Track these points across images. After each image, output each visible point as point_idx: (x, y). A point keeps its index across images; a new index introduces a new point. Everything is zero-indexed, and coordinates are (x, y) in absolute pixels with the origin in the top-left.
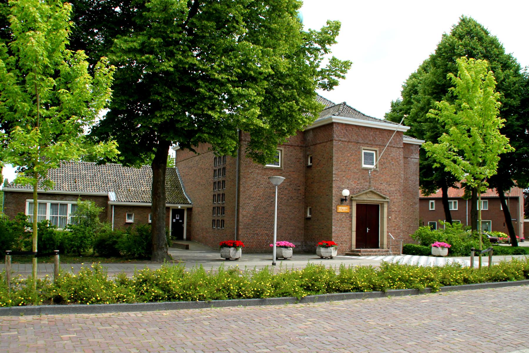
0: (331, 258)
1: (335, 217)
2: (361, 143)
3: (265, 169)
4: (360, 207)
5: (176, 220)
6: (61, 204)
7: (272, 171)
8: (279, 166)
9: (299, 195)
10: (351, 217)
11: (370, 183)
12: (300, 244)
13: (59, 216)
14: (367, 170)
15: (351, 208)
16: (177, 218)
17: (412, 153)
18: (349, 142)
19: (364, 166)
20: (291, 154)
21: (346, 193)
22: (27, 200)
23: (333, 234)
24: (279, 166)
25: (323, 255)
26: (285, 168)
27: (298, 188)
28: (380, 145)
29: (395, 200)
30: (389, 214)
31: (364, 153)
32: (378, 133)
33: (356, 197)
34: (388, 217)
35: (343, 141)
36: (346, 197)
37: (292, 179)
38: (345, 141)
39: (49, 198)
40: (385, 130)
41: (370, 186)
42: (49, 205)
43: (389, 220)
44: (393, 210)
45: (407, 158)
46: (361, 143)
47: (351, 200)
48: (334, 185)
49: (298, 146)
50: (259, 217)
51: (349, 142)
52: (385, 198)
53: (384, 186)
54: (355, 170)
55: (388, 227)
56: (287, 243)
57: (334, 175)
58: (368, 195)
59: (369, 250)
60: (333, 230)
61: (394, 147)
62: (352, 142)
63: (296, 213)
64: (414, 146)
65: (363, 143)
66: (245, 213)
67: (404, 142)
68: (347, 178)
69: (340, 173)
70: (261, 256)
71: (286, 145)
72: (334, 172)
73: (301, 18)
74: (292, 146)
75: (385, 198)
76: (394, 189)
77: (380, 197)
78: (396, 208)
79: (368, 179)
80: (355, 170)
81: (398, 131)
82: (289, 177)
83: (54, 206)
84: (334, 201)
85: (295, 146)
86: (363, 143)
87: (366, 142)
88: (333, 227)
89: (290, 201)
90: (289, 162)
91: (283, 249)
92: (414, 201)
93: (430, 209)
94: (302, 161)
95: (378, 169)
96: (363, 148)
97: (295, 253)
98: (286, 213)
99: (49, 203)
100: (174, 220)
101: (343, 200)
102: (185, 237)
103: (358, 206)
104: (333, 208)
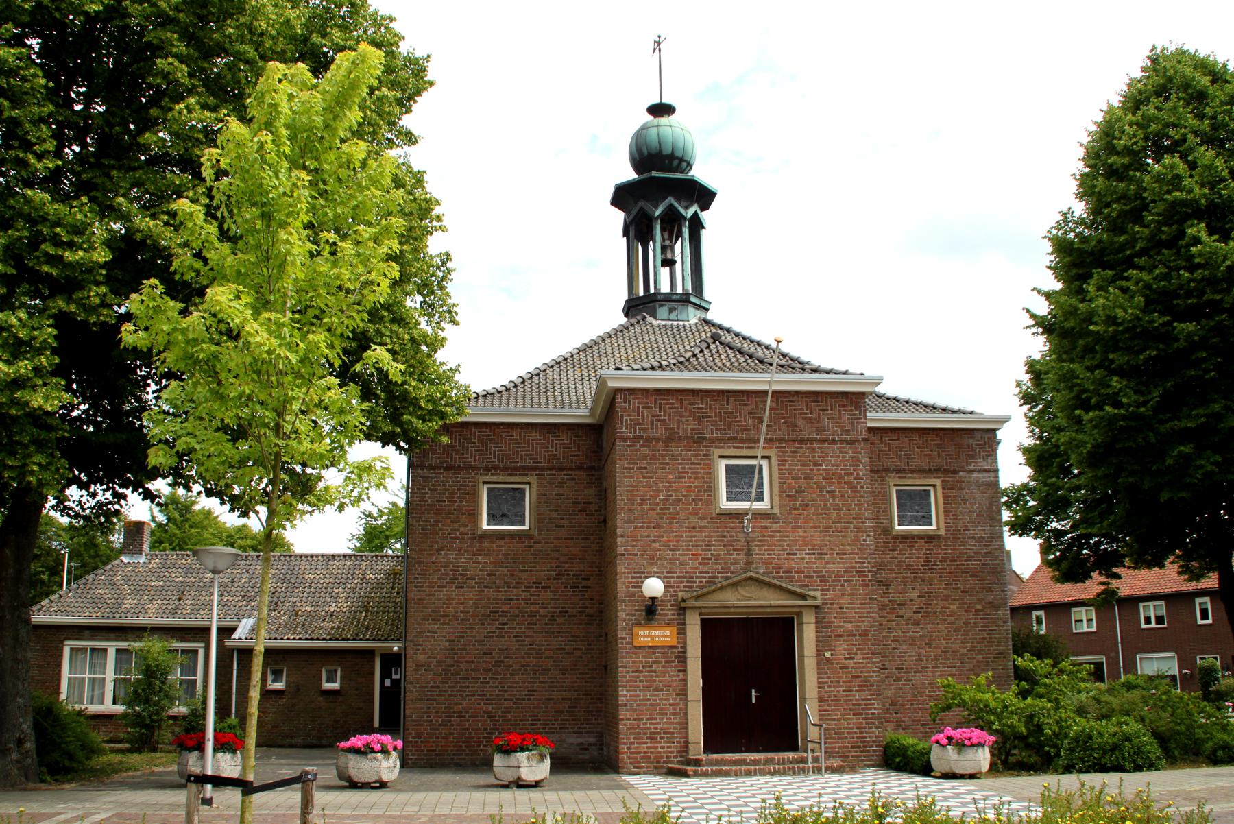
0: (382, 785)
1: (626, 663)
2: (712, 441)
3: (481, 536)
5: (393, 681)
6: (93, 650)
7: (502, 542)
8: (934, 527)
9: (587, 603)
10: (682, 657)
11: (749, 553)
12: (592, 740)
13: (87, 675)
14: (738, 515)
15: (682, 632)
16: (394, 677)
17: (973, 457)
18: (669, 439)
19: (725, 504)
20: (561, 491)
21: (654, 586)
22: (67, 643)
23: (623, 713)
24: (934, 527)
25: (356, 779)
26: (540, 530)
27: (584, 583)
28: (781, 440)
29: (846, 600)
30: (823, 643)
31: (729, 469)
33: (697, 598)
34: (819, 652)
35: (648, 440)
36: (653, 599)
37: (563, 559)
38: (657, 440)
39: (112, 636)
40: (797, 393)
41: (748, 563)
42: (111, 653)
43: (822, 662)
44: (840, 631)
45: (955, 472)
46: (712, 441)
47: (682, 610)
49: (580, 468)
50: (463, 666)
51: (669, 439)
52: (803, 597)
53: (802, 561)
54: (694, 519)
55: (820, 685)
57: (619, 540)
58: (742, 591)
59: (716, 756)
60: (622, 700)
61: (834, 442)
62: (680, 439)
63: (578, 653)
64: (978, 435)
65: (719, 440)
66: (421, 658)
67: (870, 424)
69: (643, 532)
70: (458, 778)
71: (543, 469)
73: (680, 145)
74: (561, 469)
75: (803, 597)
76: (842, 567)
78: (849, 626)
79: (741, 544)
80: (694, 519)
81: (775, 393)
82: (555, 554)
83: (124, 656)
84: (622, 615)
85: (571, 469)
86: (719, 440)
87: (732, 433)
88: (623, 692)
89: (560, 620)
90: (555, 514)
91: (351, 756)
92: (990, 599)
93: (1200, 622)
94: (593, 507)
95: (776, 511)
98: (547, 653)
99: (112, 647)
100: (388, 683)
101: (650, 610)
102: (376, 724)
103: (706, 624)
104: (621, 634)
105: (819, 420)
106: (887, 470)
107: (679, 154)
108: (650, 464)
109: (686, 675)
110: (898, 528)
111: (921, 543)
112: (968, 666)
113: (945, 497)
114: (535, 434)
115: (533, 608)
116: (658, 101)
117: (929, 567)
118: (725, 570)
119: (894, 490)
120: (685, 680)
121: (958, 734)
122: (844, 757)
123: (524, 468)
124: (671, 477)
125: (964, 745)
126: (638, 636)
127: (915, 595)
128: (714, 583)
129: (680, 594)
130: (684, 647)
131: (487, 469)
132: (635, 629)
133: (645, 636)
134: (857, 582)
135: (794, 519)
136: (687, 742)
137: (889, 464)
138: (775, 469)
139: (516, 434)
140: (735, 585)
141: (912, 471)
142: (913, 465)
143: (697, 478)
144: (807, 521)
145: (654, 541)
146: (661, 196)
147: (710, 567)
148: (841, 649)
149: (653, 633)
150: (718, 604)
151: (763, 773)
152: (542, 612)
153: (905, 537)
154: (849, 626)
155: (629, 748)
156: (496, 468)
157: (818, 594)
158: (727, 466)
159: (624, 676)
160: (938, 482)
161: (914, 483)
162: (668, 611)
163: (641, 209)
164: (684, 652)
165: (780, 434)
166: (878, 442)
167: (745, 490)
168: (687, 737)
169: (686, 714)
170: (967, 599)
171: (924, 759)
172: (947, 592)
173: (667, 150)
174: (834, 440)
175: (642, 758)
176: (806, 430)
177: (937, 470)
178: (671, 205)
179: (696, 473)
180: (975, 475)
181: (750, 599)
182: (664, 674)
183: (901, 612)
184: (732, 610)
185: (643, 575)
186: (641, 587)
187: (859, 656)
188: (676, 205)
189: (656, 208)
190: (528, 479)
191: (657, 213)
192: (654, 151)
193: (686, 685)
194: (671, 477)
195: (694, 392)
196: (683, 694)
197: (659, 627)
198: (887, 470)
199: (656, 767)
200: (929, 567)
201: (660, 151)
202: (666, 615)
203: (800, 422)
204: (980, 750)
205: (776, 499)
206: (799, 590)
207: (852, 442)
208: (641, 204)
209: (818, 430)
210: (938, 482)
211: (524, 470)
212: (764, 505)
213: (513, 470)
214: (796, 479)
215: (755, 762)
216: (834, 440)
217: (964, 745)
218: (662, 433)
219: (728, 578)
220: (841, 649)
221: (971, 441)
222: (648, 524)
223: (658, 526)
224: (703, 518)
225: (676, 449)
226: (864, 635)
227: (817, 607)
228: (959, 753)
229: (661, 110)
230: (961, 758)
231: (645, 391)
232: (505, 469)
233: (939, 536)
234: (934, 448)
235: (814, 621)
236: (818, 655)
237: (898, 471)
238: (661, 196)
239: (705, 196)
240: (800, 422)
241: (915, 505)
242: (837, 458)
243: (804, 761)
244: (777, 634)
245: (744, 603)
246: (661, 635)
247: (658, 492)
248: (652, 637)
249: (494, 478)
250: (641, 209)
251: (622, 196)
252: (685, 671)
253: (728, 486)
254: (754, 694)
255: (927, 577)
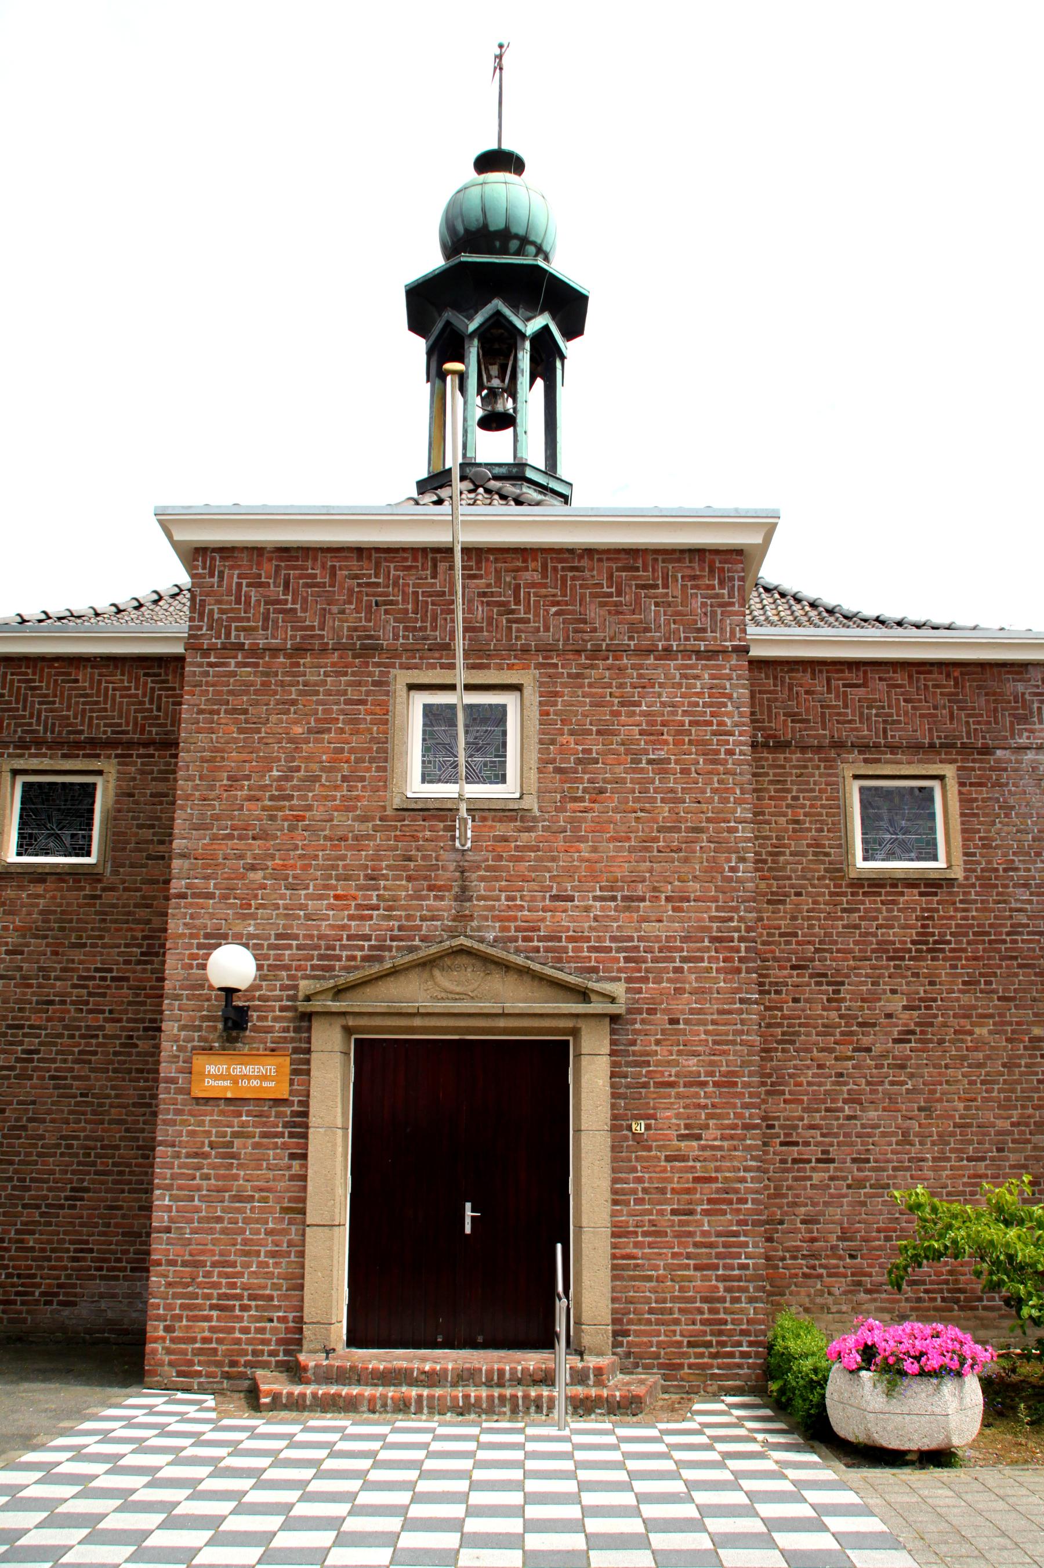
1: (176, 1132)
2: (394, 653)
4: (385, 1069)
7: (40, 889)
8: (941, 864)
10: (299, 1124)
11: (464, 895)
14: (440, 813)
15: (301, 1070)
17: (1024, 719)
18: (300, 650)
19: (415, 785)
21: (233, 965)
24: (941, 864)
26: (117, 865)
28: (547, 650)
29: (684, 1004)
30: (627, 1100)
32: (531, 576)
33: (339, 992)
34: (618, 1123)
35: (254, 651)
36: (229, 992)
38: (275, 651)
40: (590, 552)
41: (459, 917)
44: (670, 1073)
45: (986, 750)
46: (394, 653)
48: (176, 926)
51: (300, 650)
52: (584, 995)
53: (585, 916)
54: (344, 821)
55: (618, 1198)
56: (942, 1337)
58: (444, 980)
60: (159, 1218)
61: (668, 653)
62: (324, 650)
64: (1036, 675)
68: (278, 875)
71: (130, 744)
72: (178, 844)
75: (584, 995)
77: (550, 992)
78: (691, 1064)
79: (447, 874)
80: (344, 821)
82: (142, 913)
86: (411, 651)
88: (162, 1199)
90: (146, 834)
95: (531, 803)
96: (402, 678)
97: (1002, 1399)
104: (166, 1069)
105: (637, 607)
106: (839, 745)
107: (519, 229)
108: (256, 703)
109: (305, 1167)
110: (860, 863)
111: (912, 895)
112: (1013, 1158)
113: (965, 801)
114: (122, 679)
115: (91, 1020)
116: (495, 147)
117: (929, 946)
118: (405, 932)
119: (855, 786)
120: (304, 1178)
121: (889, 1336)
122: (670, 1369)
123: (93, 743)
124: (298, 730)
125: (902, 1373)
126: (203, 1075)
127: (897, 1004)
128: (380, 959)
129: (303, 984)
130: (305, 1104)
131: (22, 745)
132: (198, 1061)
133: (218, 1075)
134: (712, 962)
135: (571, 821)
136: (300, 1320)
137: (844, 733)
138: (534, 713)
139: (83, 677)
140: (428, 964)
141: (893, 748)
142: (895, 735)
143: (357, 732)
144: (599, 827)
145: (253, 868)
146: (492, 304)
147: (375, 925)
148: (671, 1115)
149: (238, 1070)
150: (381, 1007)
151: (437, 1408)
152: (110, 1028)
153: (876, 884)
154: (691, 1064)
155: (168, 1329)
156: (39, 743)
157: (618, 989)
158: (428, 709)
159: (167, 1164)
160: (949, 771)
161: (899, 773)
162: (271, 1021)
163: (448, 323)
164: (305, 1114)
165: (548, 637)
166: (820, 688)
167: (454, 755)
168: (301, 1309)
169: (302, 1254)
170: (1013, 1014)
171: (815, 1398)
172: (966, 999)
173: (497, 223)
174: (667, 649)
175: (200, 1352)
176: (603, 623)
177: (948, 746)
178: (498, 313)
179: (355, 721)
180: (1030, 756)
181: (459, 997)
182: (257, 1161)
183: (866, 1041)
184: (418, 1022)
185: (217, 938)
186: (204, 967)
187: (713, 1132)
188: (507, 312)
189: (471, 318)
190: (97, 765)
191: (472, 326)
192: (473, 226)
193: (304, 1189)
194: (298, 730)
195: (360, 552)
196: (297, 1209)
197: (253, 1056)
198: (839, 745)
199: (227, 1376)
200: (929, 946)
201: (485, 226)
202: (269, 1030)
203: (594, 612)
204: (949, 1387)
205: (533, 776)
206: (572, 979)
207: (711, 654)
208: (449, 315)
209: (634, 629)
210: (949, 771)
211: (93, 747)
212: (507, 791)
213: (73, 747)
214: (579, 733)
215: (432, 1379)
216: (667, 649)
217: (902, 1373)
218: (286, 636)
219: (412, 949)
220: (671, 1115)
221: (1020, 687)
222: (242, 831)
223: (263, 836)
224: (364, 819)
225: (311, 670)
226: (727, 1083)
227: (614, 1018)
228: (889, 1394)
229: (496, 160)
230: (895, 1406)
231: (257, 551)
232: (55, 745)
233: (951, 882)
234: (942, 701)
235: (606, 1049)
236: (614, 1128)
237: (863, 748)
238: (492, 304)
239: (569, 307)
240: (594, 612)
241: (898, 817)
242: (673, 690)
243: (547, 1379)
244: (536, 1071)
245: (440, 1007)
246: (256, 1074)
247: (268, 762)
248: (235, 1080)
249: (34, 763)
250: (448, 323)
251: (425, 303)
252: (304, 1157)
253: (426, 750)
254: (469, 1213)
255: (925, 966)
